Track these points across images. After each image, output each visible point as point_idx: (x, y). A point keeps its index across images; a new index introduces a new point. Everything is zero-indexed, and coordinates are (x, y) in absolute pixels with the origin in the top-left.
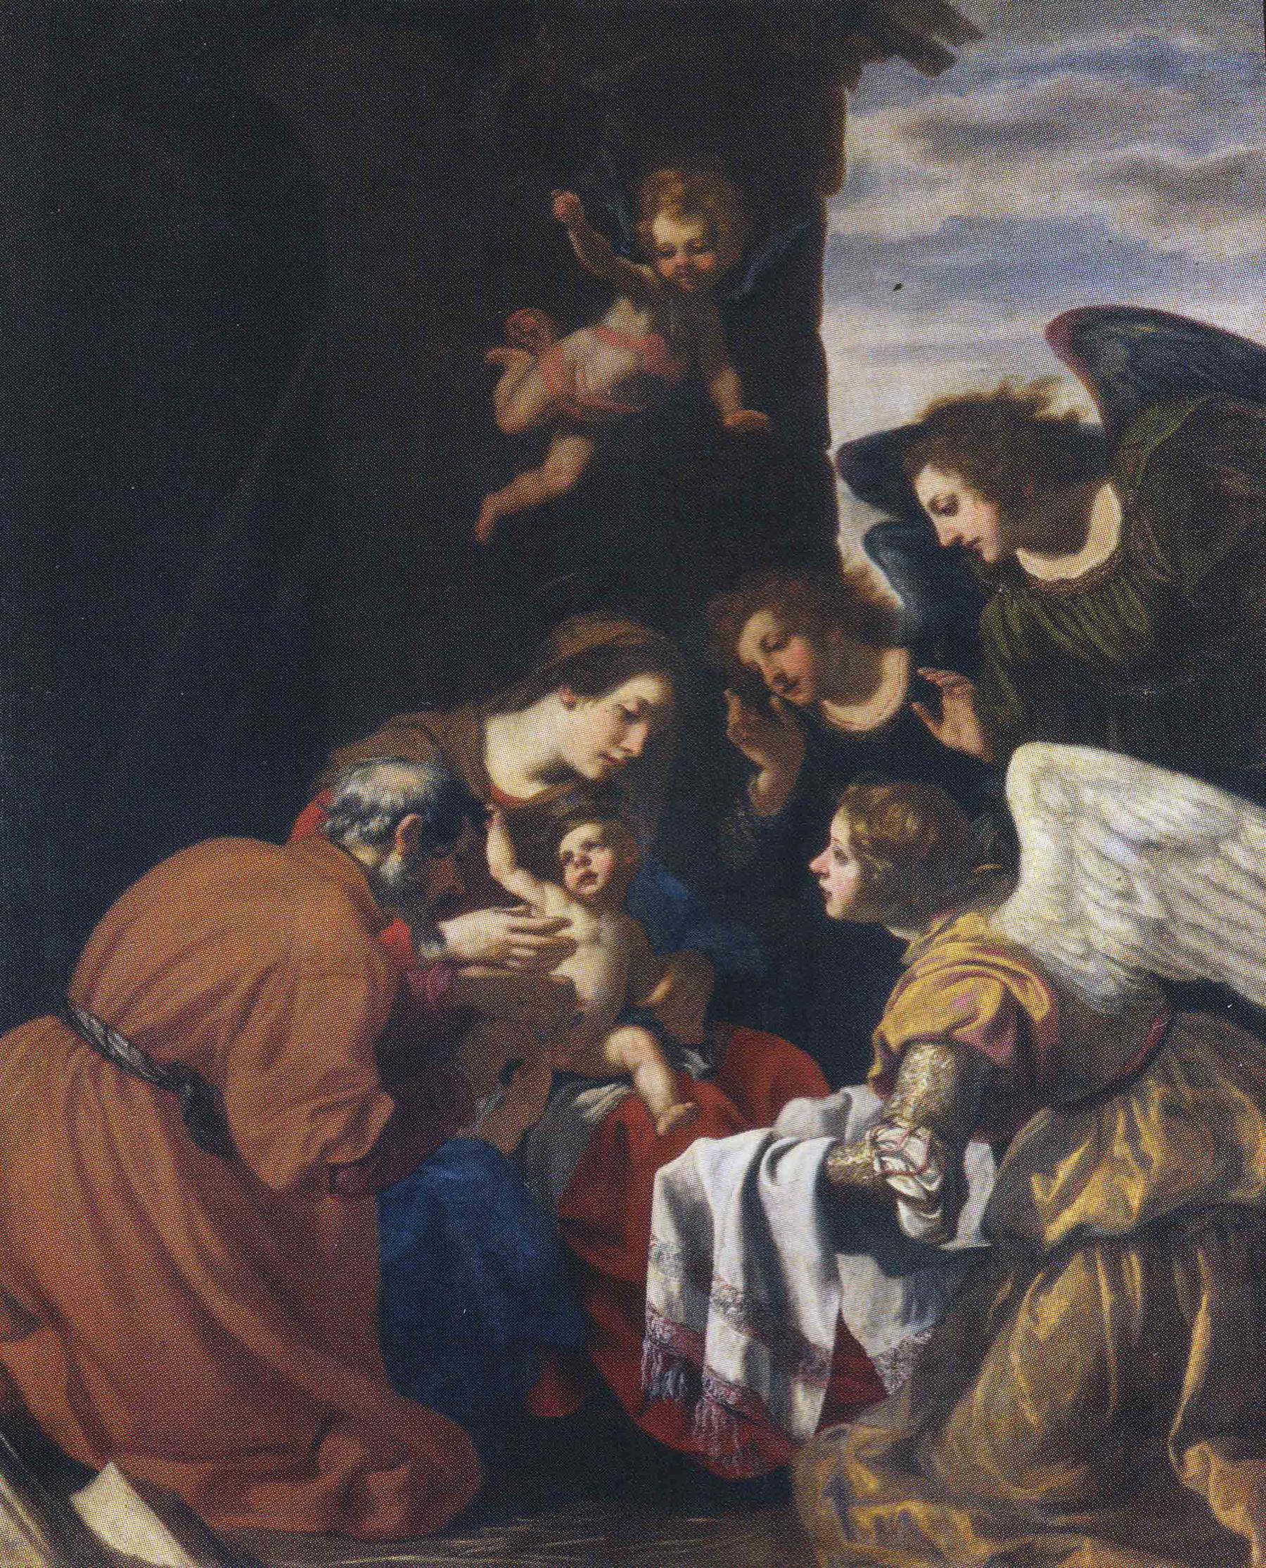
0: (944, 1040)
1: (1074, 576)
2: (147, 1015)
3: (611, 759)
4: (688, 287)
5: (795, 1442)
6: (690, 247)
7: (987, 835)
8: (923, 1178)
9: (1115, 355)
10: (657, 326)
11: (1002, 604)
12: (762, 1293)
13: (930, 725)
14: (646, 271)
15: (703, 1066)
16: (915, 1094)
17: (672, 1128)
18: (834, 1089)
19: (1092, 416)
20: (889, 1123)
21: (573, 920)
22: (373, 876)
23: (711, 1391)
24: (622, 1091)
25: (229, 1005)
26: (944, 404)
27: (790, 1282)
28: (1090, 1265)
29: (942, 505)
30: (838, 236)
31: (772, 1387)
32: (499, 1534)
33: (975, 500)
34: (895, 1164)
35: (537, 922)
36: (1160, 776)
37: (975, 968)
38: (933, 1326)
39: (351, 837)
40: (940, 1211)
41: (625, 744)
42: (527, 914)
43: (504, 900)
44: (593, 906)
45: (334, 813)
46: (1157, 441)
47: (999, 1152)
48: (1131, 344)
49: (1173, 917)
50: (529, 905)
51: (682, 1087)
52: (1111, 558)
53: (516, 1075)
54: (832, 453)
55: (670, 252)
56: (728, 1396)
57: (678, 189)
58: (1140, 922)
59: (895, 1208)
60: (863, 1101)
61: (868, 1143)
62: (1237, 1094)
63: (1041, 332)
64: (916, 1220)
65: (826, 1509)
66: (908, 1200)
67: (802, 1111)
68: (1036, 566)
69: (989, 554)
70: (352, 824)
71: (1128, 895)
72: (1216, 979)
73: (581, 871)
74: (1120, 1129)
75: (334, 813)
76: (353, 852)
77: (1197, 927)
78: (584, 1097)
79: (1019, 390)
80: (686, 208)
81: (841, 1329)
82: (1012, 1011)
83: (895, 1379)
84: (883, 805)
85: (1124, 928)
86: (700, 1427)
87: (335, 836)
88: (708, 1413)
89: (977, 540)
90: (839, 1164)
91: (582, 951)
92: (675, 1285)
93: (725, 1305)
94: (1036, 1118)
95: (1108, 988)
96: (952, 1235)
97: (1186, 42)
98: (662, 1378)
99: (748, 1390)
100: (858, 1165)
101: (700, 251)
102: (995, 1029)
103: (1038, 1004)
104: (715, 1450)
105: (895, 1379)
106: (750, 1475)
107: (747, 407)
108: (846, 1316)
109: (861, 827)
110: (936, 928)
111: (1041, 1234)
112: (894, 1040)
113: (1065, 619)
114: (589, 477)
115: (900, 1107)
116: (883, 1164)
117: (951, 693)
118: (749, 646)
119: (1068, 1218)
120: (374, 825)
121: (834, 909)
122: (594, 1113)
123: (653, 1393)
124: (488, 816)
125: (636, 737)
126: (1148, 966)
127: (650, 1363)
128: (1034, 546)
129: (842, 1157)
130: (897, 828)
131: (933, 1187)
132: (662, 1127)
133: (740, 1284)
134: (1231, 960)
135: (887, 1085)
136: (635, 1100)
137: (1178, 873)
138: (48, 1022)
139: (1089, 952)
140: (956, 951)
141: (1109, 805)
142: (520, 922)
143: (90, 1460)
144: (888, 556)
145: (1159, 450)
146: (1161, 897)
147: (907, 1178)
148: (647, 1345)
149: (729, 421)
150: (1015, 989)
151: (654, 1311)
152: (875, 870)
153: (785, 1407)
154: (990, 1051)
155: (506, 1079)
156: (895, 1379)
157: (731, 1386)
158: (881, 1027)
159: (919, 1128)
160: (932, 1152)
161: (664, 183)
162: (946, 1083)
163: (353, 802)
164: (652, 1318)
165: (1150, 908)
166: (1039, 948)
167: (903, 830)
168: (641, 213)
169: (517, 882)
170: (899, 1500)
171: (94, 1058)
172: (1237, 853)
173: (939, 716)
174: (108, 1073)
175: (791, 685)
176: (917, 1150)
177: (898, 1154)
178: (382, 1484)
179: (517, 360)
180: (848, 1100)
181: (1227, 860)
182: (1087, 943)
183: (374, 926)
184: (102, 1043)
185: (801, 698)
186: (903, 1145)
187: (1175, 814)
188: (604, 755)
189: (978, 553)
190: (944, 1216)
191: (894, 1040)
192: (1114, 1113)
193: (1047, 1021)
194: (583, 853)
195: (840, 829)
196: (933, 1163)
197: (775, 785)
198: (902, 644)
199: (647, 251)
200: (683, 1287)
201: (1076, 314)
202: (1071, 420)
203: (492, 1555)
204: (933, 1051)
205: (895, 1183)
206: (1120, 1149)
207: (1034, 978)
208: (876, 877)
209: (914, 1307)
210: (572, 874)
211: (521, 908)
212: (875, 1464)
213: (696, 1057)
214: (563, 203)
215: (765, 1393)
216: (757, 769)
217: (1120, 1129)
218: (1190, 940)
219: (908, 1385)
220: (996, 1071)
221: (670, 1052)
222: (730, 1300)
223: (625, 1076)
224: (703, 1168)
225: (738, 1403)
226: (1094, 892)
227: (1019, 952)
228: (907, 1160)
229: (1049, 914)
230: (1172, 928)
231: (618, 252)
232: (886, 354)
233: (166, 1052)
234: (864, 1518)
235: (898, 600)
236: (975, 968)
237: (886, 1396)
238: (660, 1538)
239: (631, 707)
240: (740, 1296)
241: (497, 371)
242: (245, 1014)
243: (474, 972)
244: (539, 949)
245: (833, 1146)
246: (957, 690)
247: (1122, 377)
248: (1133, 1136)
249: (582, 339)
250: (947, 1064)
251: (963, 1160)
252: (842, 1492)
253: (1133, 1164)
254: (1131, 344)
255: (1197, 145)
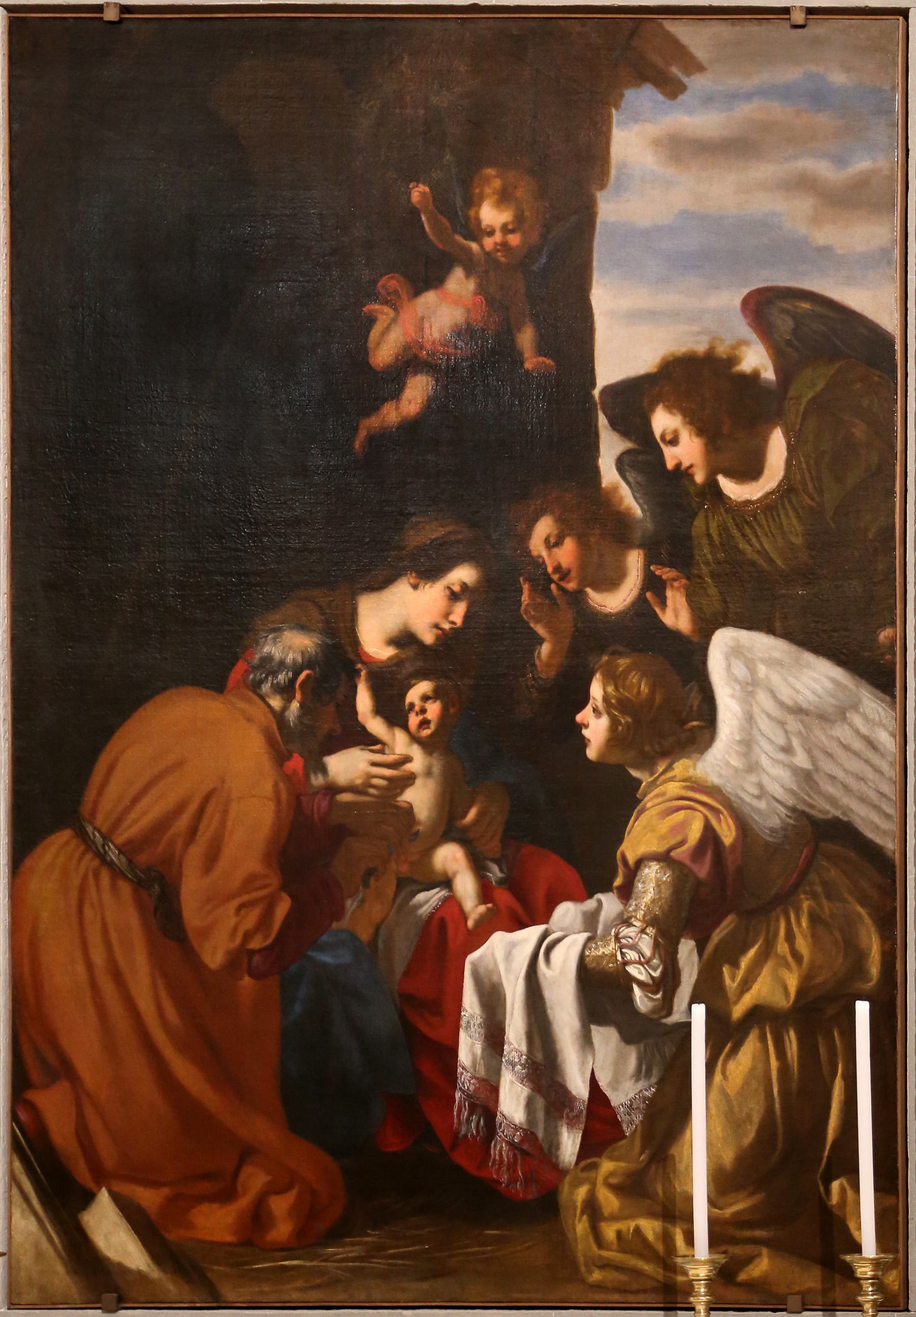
0: (664, 858)
1: (755, 498)
2: (129, 831)
3: (441, 629)
4: (503, 259)
5: (561, 1172)
6: (505, 229)
7: (695, 700)
8: (650, 967)
9: (784, 325)
10: (481, 289)
11: (707, 517)
12: (539, 1056)
13: (658, 610)
14: (474, 246)
15: (499, 875)
16: (645, 900)
17: (479, 923)
18: (590, 896)
19: (769, 374)
20: (627, 923)
21: (411, 754)
22: (280, 717)
23: (503, 1132)
24: (443, 893)
25: (183, 822)
26: (671, 358)
27: (558, 1047)
28: (763, 1038)
29: (668, 438)
30: (605, 223)
31: (545, 1129)
32: (358, 1244)
33: (690, 436)
34: (632, 955)
35: (389, 758)
36: (809, 657)
37: (683, 803)
38: (656, 1083)
39: (266, 688)
40: (661, 993)
41: (452, 618)
42: (382, 752)
43: (367, 740)
44: (427, 745)
45: (255, 668)
46: (810, 395)
47: (701, 949)
48: (795, 316)
49: (817, 769)
50: (383, 744)
51: (485, 893)
52: (779, 486)
53: (372, 881)
54: (596, 393)
55: (491, 233)
56: (514, 1135)
57: (497, 183)
58: (796, 771)
59: (632, 989)
60: (609, 903)
61: (613, 940)
62: (859, 909)
63: (737, 302)
64: (646, 999)
65: (581, 1227)
66: (641, 984)
67: (568, 911)
68: (728, 486)
69: (699, 477)
70: (266, 678)
71: (787, 750)
72: (845, 819)
73: (421, 717)
74: (782, 932)
75: (255, 668)
76: (267, 699)
77: (832, 778)
78: (421, 897)
79: (722, 350)
80: (504, 198)
81: (594, 1083)
82: (710, 835)
83: (631, 1122)
84: (626, 672)
85: (784, 774)
86: (495, 1160)
87: (256, 686)
88: (500, 1149)
89: (691, 466)
90: (593, 954)
91: (419, 782)
92: (478, 1048)
93: (513, 1064)
94: (725, 923)
95: (775, 822)
96: (670, 1012)
97: (838, 78)
98: (468, 1121)
99: (529, 1134)
100: (606, 955)
101: (512, 231)
102: (699, 851)
103: (727, 833)
104: (505, 1178)
105: (631, 1123)
106: (530, 1197)
107: (540, 355)
108: (597, 1074)
109: (610, 689)
110: (661, 770)
111: (729, 1014)
112: (631, 859)
113: (748, 531)
114: (431, 406)
115: (635, 911)
116: (622, 954)
117: (672, 586)
118: (537, 544)
119: (747, 1000)
120: (281, 677)
121: (592, 753)
122: (425, 911)
123: (463, 1133)
124: (358, 672)
125: (459, 612)
126: (801, 807)
127: (460, 1111)
128: (729, 474)
129: (595, 949)
130: (635, 691)
131: (656, 974)
132: (470, 923)
133: (524, 1048)
134: (854, 805)
135: (626, 893)
136: (452, 902)
137: (820, 735)
138: (65, 835)
139: (763, 793)
140: (673, 788)
141: (776, 679)
142: (378, 758)
143: (90, 1184)
144: (631, 476)
145: (813, 400)
146: (809, 752)
147: (639, 966)
148: (458, 1095)
149: (528, 365)
150: (714, 823)
151: (463, 1068)
152: (620, 723)
153: (555, 1144)
154: (695, 868)
155: (366, 884)
156: (631, 1123)
157: (516, 1128)
158: (623, 847)
159: (647, 926)
160: (656, 946)
161: (488, 180)
162: (666, 893)
163: (269, 658)
164: (462, 1073)
165: (801, 760)
166: (729, 788)
167: (639, 692)
168: (472, 202)
169: (376, 726)
170: (632, 1217)
171: (96, 863)
172: (858, 721)
173: (663, 603)
174: (105, 877)
175: (565, 575)
176: (646, 945)
177: (633, 947)
178: (280, 1205)
179: (384, 313)
180: (600, 903)
181: (851, 725)
182: (760, 786)
183: (280, 758)
184: (102, 851)
185: (571, 586)
186: (637, 940)
187: (818, 687)
188: (437, 626)
189: (691, 477)
190: (664, 997)
191: (631, 859)
192: (778, 921)
193: (733, 846)
194: (422, 704)
195: (596, 690)
196: (657, 956)
197: (552, 654)
198: (641, 546)
199: (476, 232)
200: (483, 1050)
201: (759, 291)
202: (755, 376)
203: (353, 1260)
204: (658, 866)
205: (632, 970)
206: (782, 947)
207: (725, 812)
208: (620, 728)
209: (644, 1068)
210: (414, 720)
211: (378, 747)
212: (617, 1189)
213: (495, 868)
214: (418, 193)
215: (540, 1134)
216: (540, 641)
217: (782, 932)
218: (830, 789)
219: (639, 1128)
220: (699, 883)
221: (477, 865)
222: (517, 1060)
223: (447, 882)
224: (500, 956)
225: (522, 1141)
226: (767, 747)
227: (714, 791)
228: (640, 953)
229: (736, 762)
230: (816, 777)
231: (455, 231)
232: (634, 316)
233: (142, 859)
234: (610, 1232)
235: (638, 511)
236: (683, 803)
237: (625, 1137)
238: (467, 1247)
239: (457, 588)
240: (524, 1057)
241: (371, 321)
242: (193, 831)
243: (346, 797)
244: (389, 779)
245: (589, 939)
246: (676, 584)
247: (789, 343)
248: (790, 938)
249: (430, 297)
250: (667, 877)
251: (677, 953)
252: (592, 1208)
253: (790, 959)
254: (795, 316)
255: (841, 161)
